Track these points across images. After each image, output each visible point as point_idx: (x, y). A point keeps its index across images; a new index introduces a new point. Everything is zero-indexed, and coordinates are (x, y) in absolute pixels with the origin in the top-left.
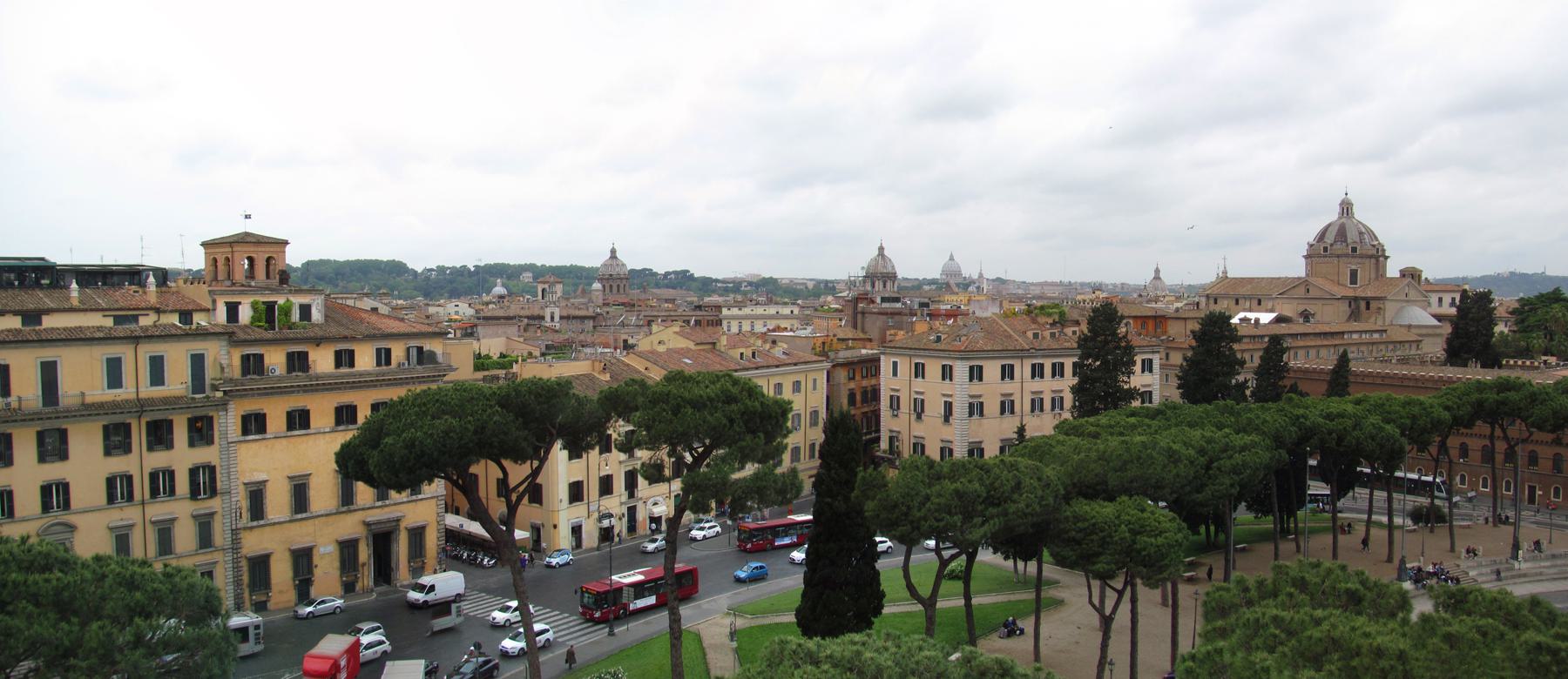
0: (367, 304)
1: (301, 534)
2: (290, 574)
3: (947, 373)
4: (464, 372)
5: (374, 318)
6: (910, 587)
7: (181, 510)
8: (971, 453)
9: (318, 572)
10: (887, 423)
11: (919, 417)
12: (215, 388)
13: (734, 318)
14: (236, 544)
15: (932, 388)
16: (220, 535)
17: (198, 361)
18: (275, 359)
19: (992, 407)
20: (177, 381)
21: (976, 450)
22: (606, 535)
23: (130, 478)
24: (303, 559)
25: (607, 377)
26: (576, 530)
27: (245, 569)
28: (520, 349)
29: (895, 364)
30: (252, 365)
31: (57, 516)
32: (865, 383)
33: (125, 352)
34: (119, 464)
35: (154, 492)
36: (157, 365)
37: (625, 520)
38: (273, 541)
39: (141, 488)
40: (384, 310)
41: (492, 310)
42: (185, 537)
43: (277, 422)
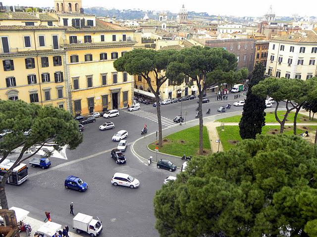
0: (109, 20)
1: (90, 94)
2: (87, 106)
3: (292, 49)
4: (140, 45)
5: (111, 25)
6: (276, 117)
7: (52, 86)
8: (296, 76)
9: (95, 105)
10: (269, 64)
11: (289, 65)
12: (61, 47)
13: (222, 28)
14: (70, 97)
15: (286, 54)
16: (65, 94)
17: (55, 38)
18: (81, 38)
19: (306, 62)
20: (49, 44)
21: (298, 76)
22: (179, 95)
23: (35, 76)
24: (91, 101)
25: (183, 46)
26: (170, 94)
27: (73, 104)
28: (156, 37)
29: (274, 45)
30: (73, 40)
31: (12, 88)
32: (263, 51)
33: (30, 34)
34: (31, 72)
35: (43, 81)
36: (42, 39)
37: (184, 91)
38: (82, 95)
39: (39, 79)
40: (114, 22)
41: (144, 24)
42: (54, 94)
43: (82, 59)
